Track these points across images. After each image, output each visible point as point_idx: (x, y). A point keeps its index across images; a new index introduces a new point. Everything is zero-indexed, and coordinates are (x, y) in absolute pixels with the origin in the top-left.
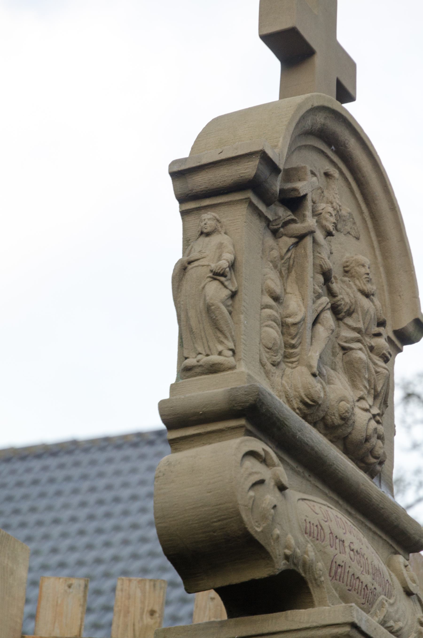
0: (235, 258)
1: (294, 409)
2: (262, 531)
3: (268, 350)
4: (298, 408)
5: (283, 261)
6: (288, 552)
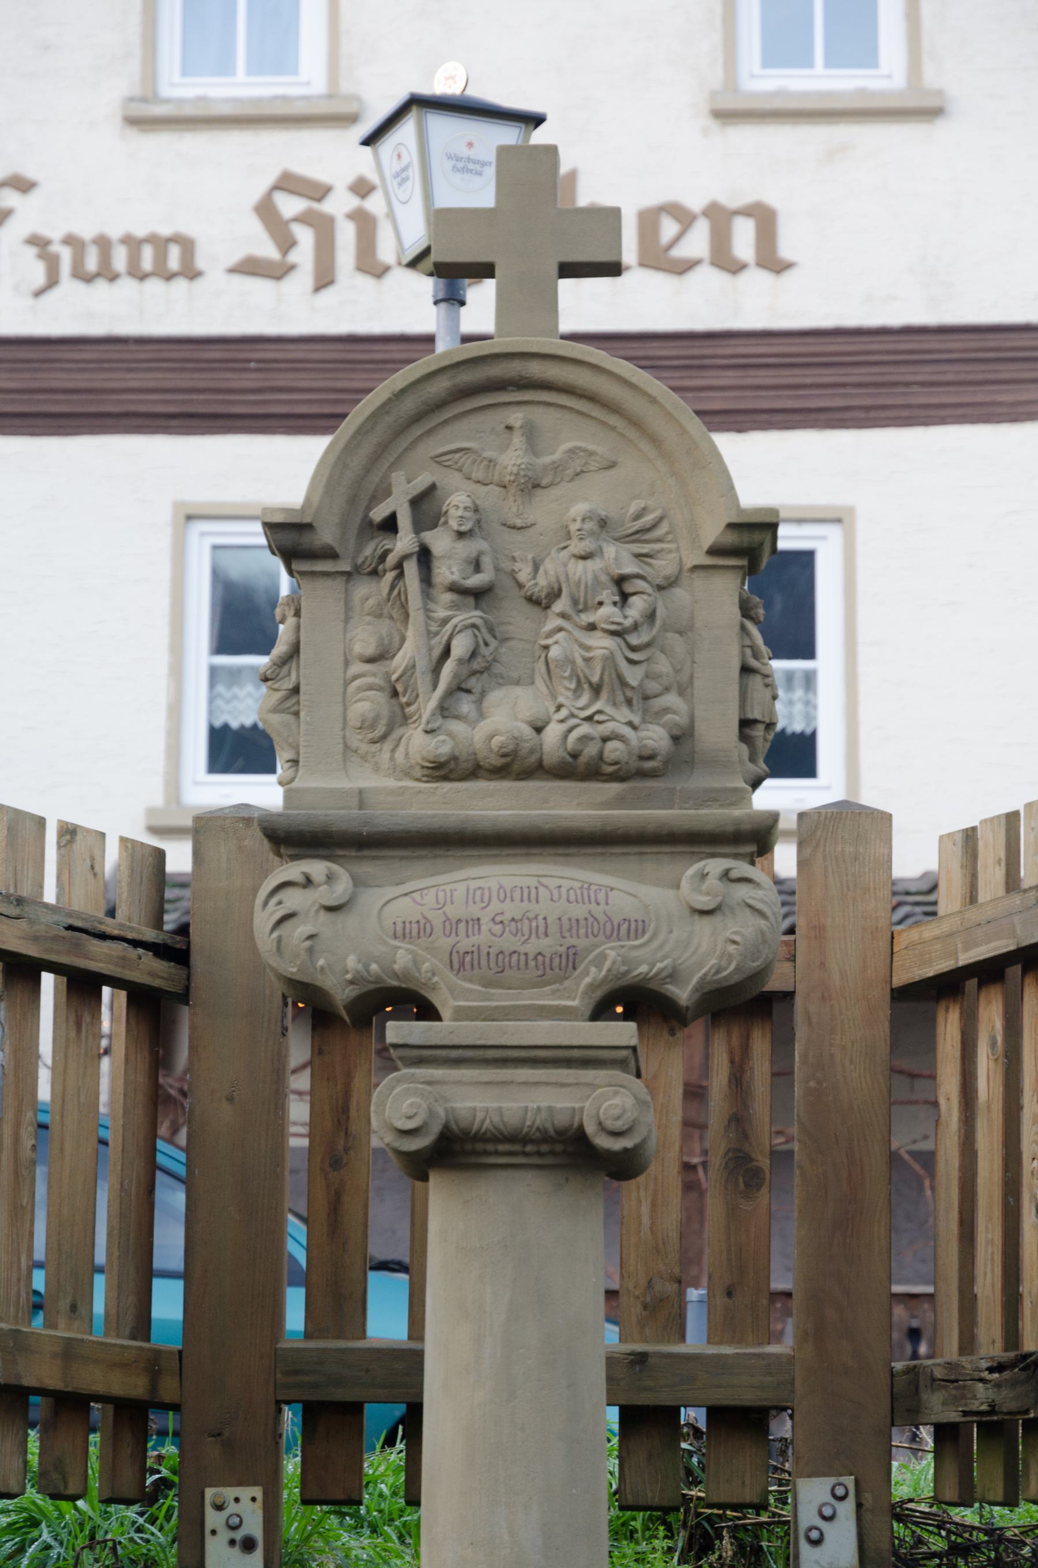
0: (345, 630)
1: (418, 780)
2: (299, 970)
3: (359, 731)
4: (423, 776)
5: (390, 603)
6: (349, 976)
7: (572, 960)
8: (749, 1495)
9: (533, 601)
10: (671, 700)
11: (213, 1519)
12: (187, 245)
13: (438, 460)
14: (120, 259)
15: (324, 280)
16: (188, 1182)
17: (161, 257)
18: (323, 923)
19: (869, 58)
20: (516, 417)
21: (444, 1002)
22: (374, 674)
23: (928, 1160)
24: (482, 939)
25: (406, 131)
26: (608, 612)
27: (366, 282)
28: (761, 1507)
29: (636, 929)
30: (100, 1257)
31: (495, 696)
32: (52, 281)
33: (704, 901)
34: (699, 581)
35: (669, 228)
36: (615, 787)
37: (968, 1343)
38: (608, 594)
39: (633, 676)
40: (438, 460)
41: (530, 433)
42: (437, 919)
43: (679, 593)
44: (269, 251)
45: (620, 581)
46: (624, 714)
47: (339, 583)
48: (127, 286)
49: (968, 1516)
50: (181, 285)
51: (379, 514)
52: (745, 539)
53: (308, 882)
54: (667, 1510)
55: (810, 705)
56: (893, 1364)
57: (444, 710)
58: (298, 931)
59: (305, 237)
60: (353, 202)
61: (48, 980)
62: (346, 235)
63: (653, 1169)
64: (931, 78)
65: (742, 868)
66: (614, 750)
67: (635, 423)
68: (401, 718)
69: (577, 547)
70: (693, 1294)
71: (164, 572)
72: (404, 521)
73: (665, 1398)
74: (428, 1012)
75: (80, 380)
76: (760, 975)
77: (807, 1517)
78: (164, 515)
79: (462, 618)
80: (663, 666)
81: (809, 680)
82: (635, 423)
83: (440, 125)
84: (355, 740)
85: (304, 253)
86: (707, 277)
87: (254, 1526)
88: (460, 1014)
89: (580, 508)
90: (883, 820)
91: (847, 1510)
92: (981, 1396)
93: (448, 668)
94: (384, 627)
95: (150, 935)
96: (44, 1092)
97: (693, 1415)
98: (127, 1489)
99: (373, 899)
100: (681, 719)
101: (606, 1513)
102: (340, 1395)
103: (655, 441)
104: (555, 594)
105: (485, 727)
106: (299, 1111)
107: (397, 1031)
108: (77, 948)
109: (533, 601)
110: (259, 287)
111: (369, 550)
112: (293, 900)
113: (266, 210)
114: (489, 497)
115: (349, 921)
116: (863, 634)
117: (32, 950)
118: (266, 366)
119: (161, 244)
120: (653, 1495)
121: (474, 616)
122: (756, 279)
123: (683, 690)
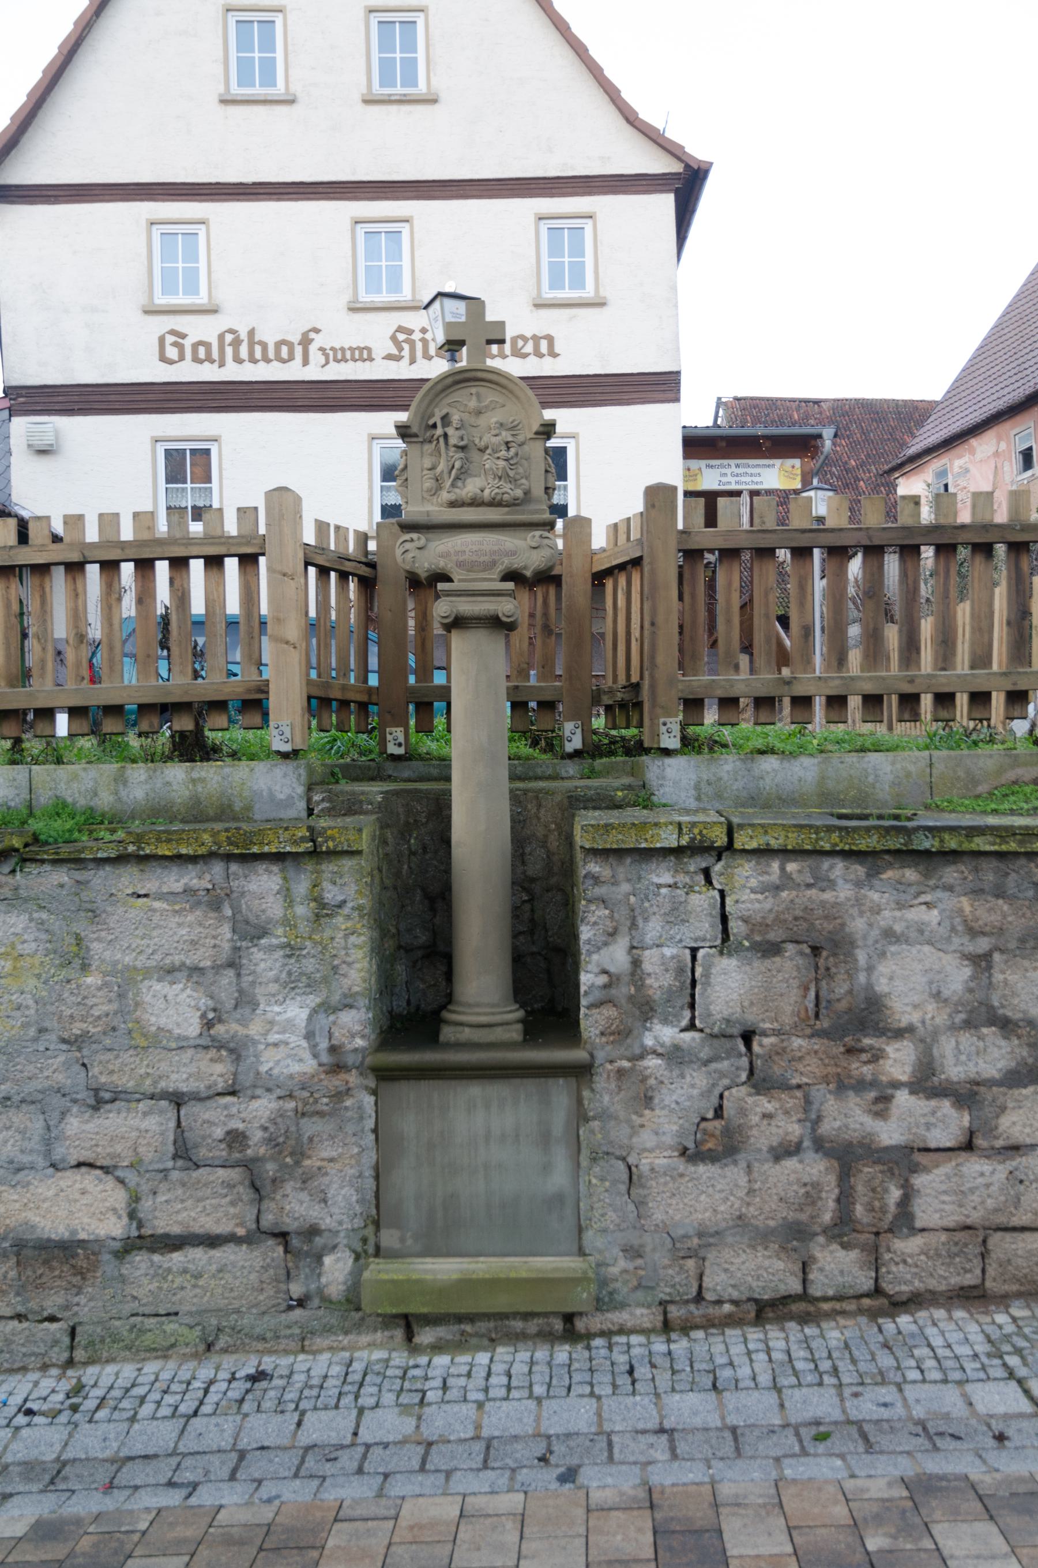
7: (494, 563)
8: (550, 727)
9: (480, 450)
10: (524, 481)
11: (389, 737)
12: (369, 350)
13: (449, 405)
14: (348, 355)
15: (413, 361)
16: (379, 644)
17: (361, 354)
18: (417, 553)
19: (582, 286)
20: (473, 390)
21: (455, 576)
22: (431, 474)
23: (602, 635)
24: (466, 557)
25: (437, 305)
26: (503, 453)
27: (425, 361)
28: (553, 731)
29: (513, 553)
30: (352, 666)
31: (469, 481)
32: (327, 363)
33: (534, 544)
34: (532, 443)
35: (520, 343)
36: (506, 509)
37: (615, 680)
38: (503, 447)
39: (511, 473)
40: (449, 405)
41: (478, 395)
42: (452, 551)
43: (526, 447)
44: (395, 352)
45: (507, 443)
46: (509, 486)
47: (418, 446)
48: (351, 363)
49: (614, 732)
50: (368, 363)
51: (431, 422)
52: (546, 429)
53: (412, 540)
54: (525, 733)
55: (566, 496)
56: (607, 912)
57: (453, 485)
58: (410, 555)
59: (406, 346)
60: (421, 335)
61: (333, 574)
62: (419, 346)
63: (519, 629)
64: (602, 293)
65: (546, 534)
66: (506, 497)
67: (511, 392)
68: (440, 488)
69: (494, 432)
70: (532, 672)
71: (366, 456)
72: (439, 425)
73: (524, 699)
74: (449, 580)
75: (338, 394)
76: (551, 568)
77: (567, 733)
78: (365, 438)
79: (458, 455)
80: (521, 470)
81: (565, 488)
82: (511, 392)
83: (448, 303)
84: (425, 495)
85: (406, 353)
86: (532, 358)
87: (401, 739)
88: (460, 580)
89: (494, 420)
90: (588, 521)
91: (579, 731)
92: (619, 696)
93: (454, 472)
94: (434, 459)
95: (364, 560)
96: (333, 618)
97: (533, 705)
98: (363, 729)
99: (432, 545)
100: (526, 487)
101: (507, 734)
102: (426, 700)
103: (517, 398)
104: (487, 448)
105: (466, 490)
106: (411, 623)
107: (440, 586)
108: (341, 564)
109: (480, 450)
110: (392, 364)
111: (428, 434)
112: (408, 546)
113: (393, 338)
114: (466, 417)
115: (425, 552)
116: (582, 473)
117: (327, 564)
118: (395, 389)
119: (361, 349)
120: (521, 728)
121: (461, 455)
122: (548, 359)
123: (527, 478)
